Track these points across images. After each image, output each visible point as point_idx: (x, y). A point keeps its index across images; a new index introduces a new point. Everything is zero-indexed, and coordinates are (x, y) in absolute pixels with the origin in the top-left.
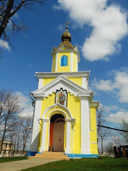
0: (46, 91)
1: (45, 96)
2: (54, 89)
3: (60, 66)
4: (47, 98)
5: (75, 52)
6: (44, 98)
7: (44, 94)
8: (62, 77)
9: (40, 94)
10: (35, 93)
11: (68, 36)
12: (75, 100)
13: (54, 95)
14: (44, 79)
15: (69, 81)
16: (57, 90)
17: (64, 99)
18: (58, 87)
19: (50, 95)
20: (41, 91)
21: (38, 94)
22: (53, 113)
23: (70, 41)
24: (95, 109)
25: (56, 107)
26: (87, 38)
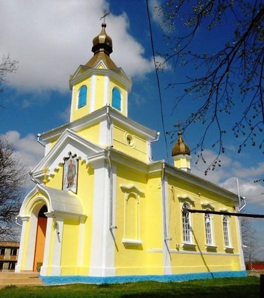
0: (50, 165)
1: (49, 174)
2: (60, 159)
3: (77, 108)
4: (52, 176)
5: (101, 73)
6: (49, 178)
7: (46, 170)
8: (68, 131)
9: (41, 172)
10: (36, 171)
11: (100, 42)
12: (88, 172)
13: (61, 168)
14: (52, 143)
15: (77, 136)
16: (66, 159)
17: (74, 173)
18: (64, 154)
19: (57, 170)
20: (44, 165)
21: (40, 172)
22: (34, 206)
23: (225, 132)
24: (160, 178)
25: (38, 193)
26: (143, 51)
